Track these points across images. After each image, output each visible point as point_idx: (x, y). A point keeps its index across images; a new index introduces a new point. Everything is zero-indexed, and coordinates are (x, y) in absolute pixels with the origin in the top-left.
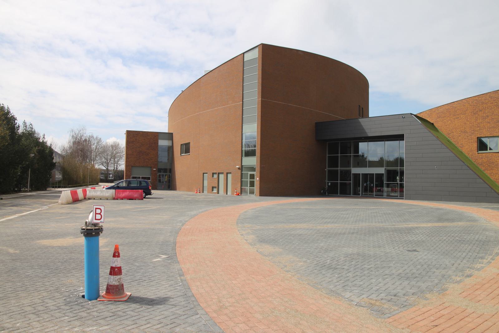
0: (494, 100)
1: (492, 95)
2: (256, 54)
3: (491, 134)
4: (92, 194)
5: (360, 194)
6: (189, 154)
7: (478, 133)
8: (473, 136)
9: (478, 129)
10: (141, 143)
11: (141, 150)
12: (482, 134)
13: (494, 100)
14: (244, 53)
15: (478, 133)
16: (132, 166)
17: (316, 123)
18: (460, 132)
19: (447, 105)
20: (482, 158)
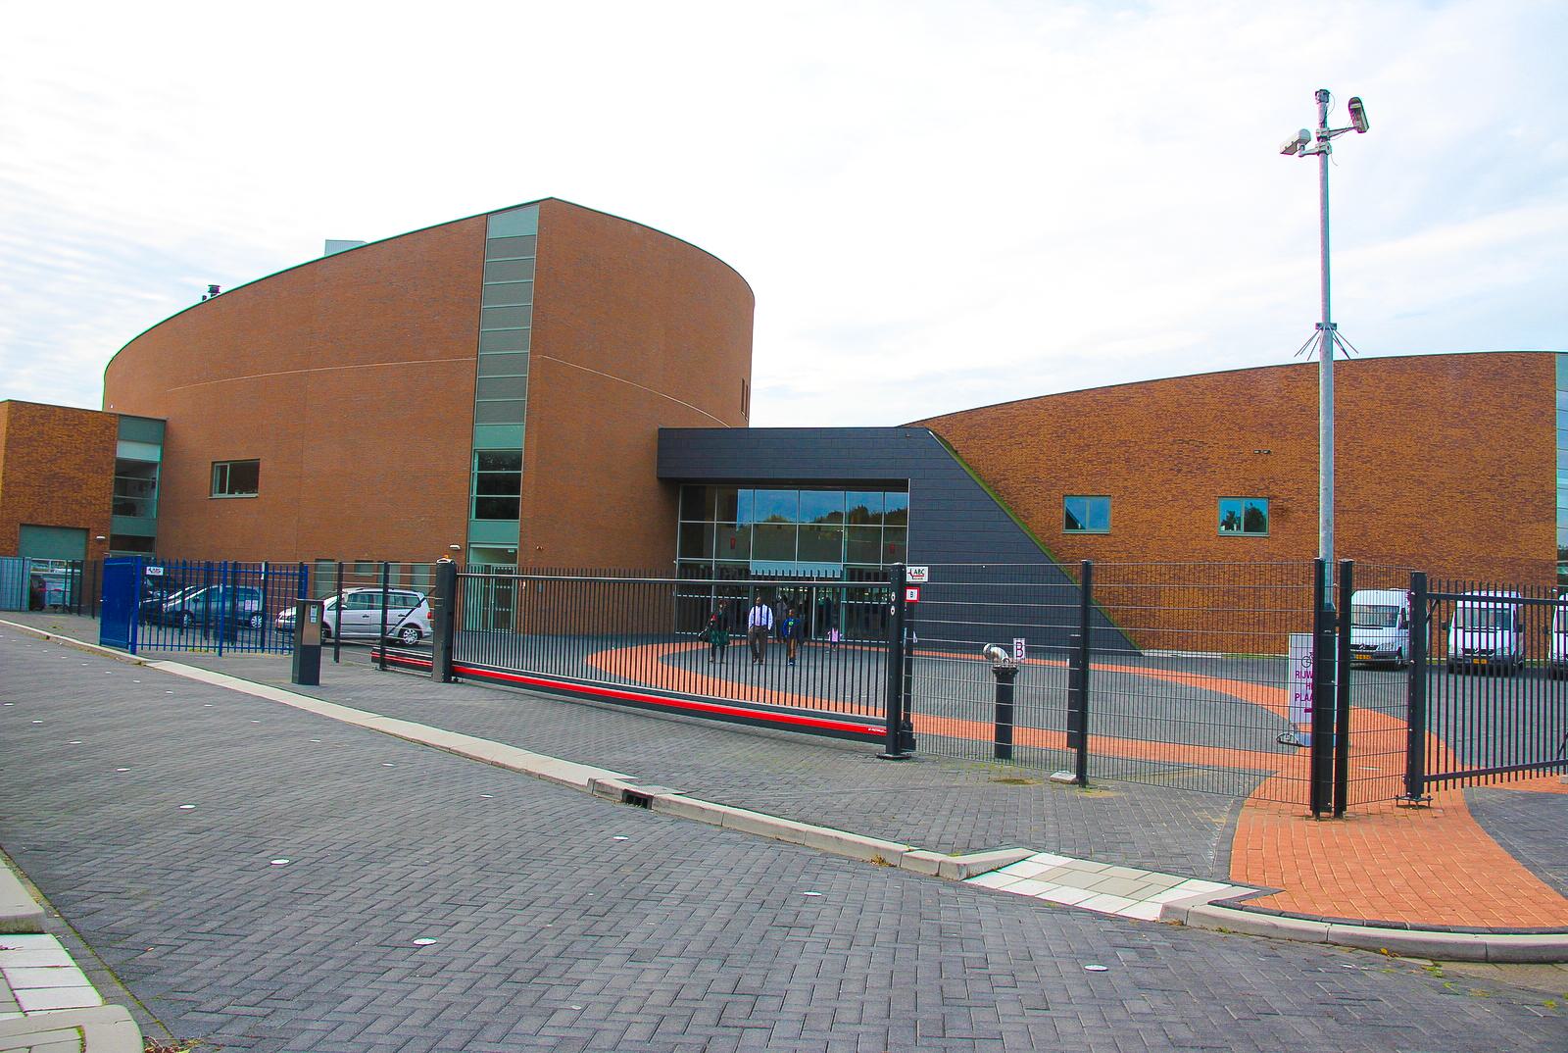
0: (1104, 410)
1: (1098, 397)
2: (530, 226)
3: (1093, 490)
4: (547, 711)
5: (1331, 808)
6: (254, 495)
7: (1065, 486)
8: (1053, 492)
9: (1067, 474)
10: (57, 447)
11: (58, 470)
12: (1075, 489)
13: (1104, 410)
14: (487, 214)
15: (1065, 486)
16: (22, 525)
17: (663, 433)
18: (1023, 480)
19: (994, 409)
20: (1073, 547)
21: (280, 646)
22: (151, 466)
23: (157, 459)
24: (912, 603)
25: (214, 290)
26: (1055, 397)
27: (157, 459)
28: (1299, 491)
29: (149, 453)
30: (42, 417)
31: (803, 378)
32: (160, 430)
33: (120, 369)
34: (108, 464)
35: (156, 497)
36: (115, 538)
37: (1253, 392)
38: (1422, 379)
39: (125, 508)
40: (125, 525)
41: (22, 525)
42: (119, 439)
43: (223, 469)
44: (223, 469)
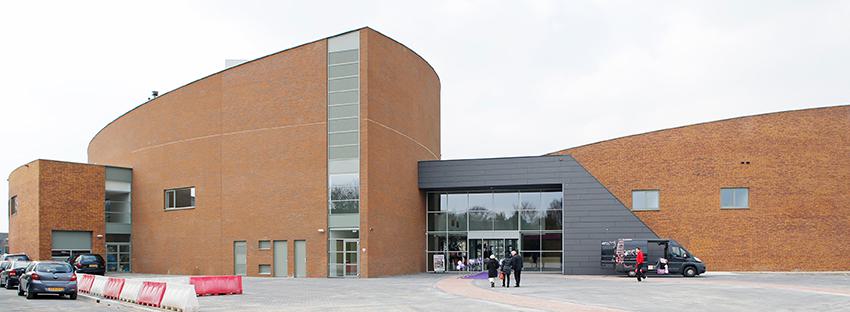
21: (334, 266)
22: (126, 194)
23: (129, 190)
24: (755, 198)
25: (155, 94)
26: (660, 134)
27: (129, 190)
28: (766, 184)
29: (126, 188)
30: (60, 168)
31: (465, 134)
32: (129, 173)
33: (97, 143)
34: (101, 194)
35: (130, 211)
36: (107, 235)
37: (740, 130)
38: (833, 120)
39: (110, 219)
40: (113, 228)
41: (53, 231)
42: (109, 180)
43: (171, 194)
44: (171, 194)
